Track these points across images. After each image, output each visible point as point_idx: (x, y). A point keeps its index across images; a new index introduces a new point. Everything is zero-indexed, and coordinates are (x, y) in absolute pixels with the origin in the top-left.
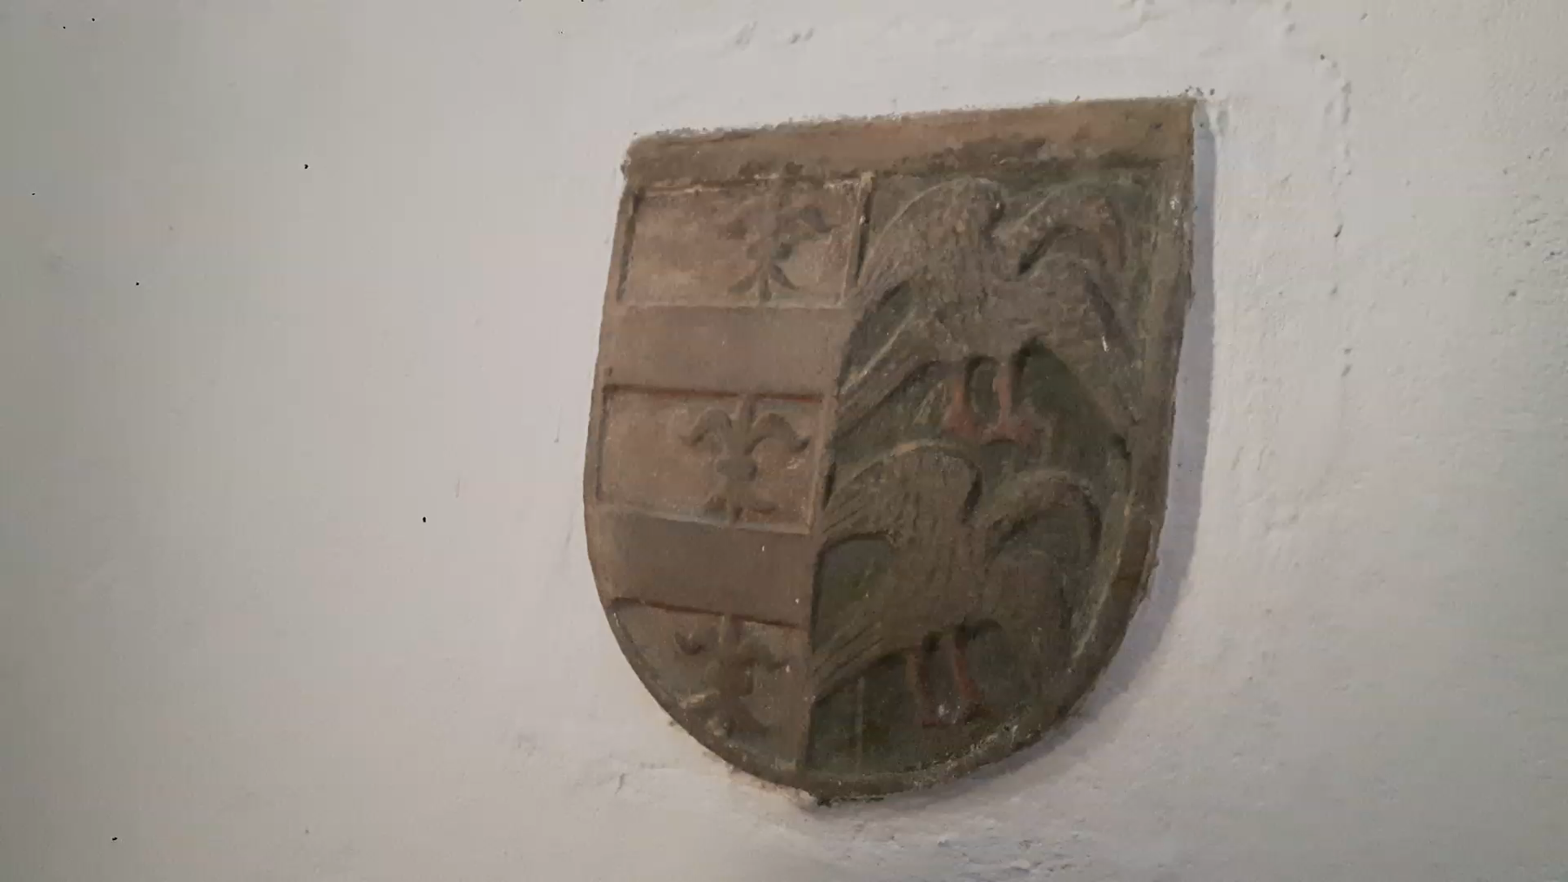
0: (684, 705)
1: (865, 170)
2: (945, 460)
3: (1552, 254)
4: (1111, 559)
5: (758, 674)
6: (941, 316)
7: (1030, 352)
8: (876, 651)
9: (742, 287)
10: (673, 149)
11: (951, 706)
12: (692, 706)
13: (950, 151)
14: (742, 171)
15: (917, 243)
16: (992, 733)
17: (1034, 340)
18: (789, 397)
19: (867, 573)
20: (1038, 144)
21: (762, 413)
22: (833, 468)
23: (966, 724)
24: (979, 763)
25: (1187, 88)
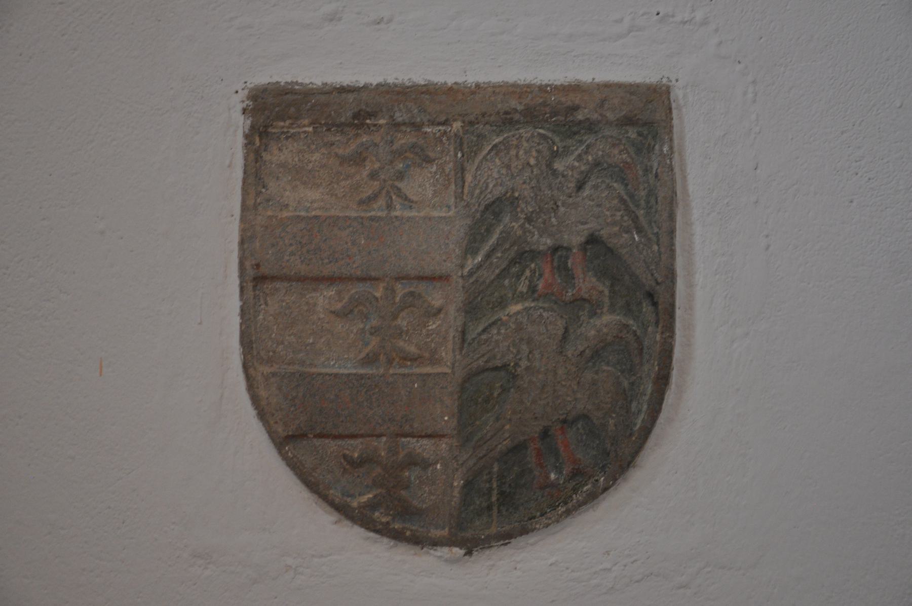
0: (355, 504)
1: (455, 120)
2: (545, 314)
3: (869, 179)
4: (650, 369)
5: (411, 474)
6: (529, 220)
7: (593, 240)
8: (507, 443)
9: (366, 202)
10: (289, 97)
11: (559, 470)
12: (361, 504)
13: (515, 110)
14: (356, 116)
15: (504, 171)
16: (587, 485)
17: (592, 235)
18: (421, 278)
19: (495, 394)
20: (575, 108)
21: (401, 290)
22: (465, 324)
23: (569, 482)
24: (580, 504)
25: (661, 77)
